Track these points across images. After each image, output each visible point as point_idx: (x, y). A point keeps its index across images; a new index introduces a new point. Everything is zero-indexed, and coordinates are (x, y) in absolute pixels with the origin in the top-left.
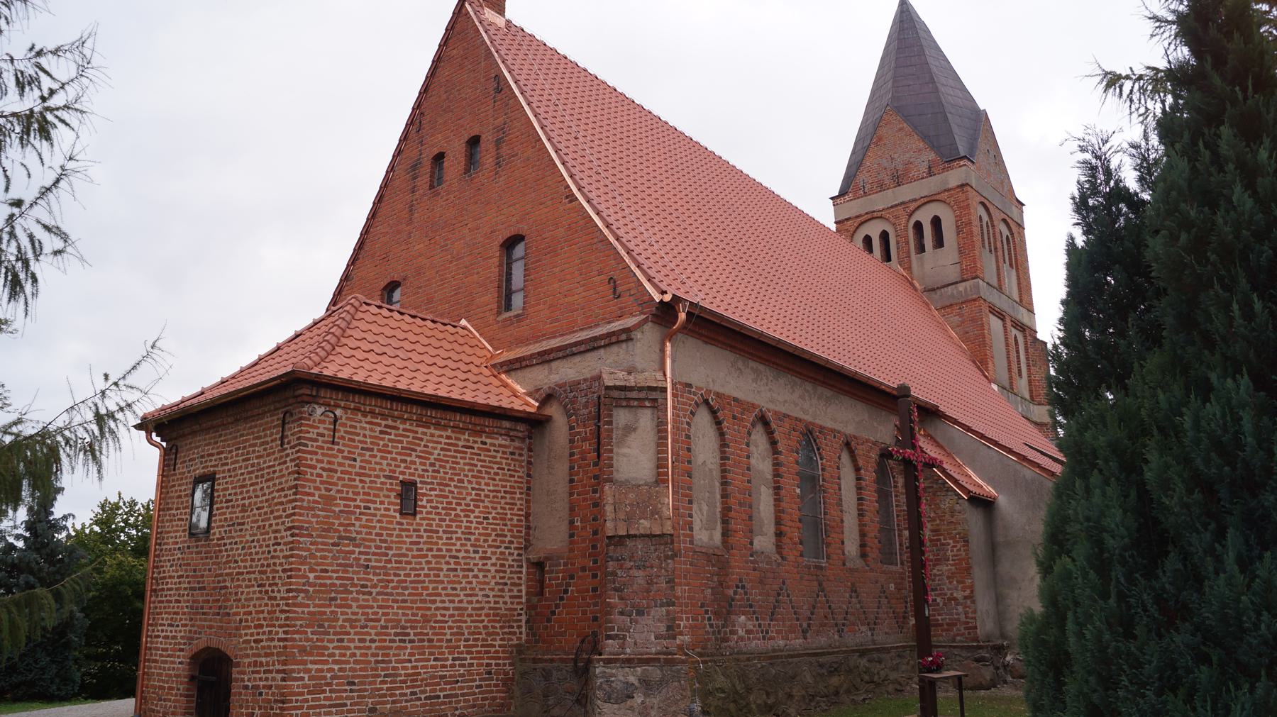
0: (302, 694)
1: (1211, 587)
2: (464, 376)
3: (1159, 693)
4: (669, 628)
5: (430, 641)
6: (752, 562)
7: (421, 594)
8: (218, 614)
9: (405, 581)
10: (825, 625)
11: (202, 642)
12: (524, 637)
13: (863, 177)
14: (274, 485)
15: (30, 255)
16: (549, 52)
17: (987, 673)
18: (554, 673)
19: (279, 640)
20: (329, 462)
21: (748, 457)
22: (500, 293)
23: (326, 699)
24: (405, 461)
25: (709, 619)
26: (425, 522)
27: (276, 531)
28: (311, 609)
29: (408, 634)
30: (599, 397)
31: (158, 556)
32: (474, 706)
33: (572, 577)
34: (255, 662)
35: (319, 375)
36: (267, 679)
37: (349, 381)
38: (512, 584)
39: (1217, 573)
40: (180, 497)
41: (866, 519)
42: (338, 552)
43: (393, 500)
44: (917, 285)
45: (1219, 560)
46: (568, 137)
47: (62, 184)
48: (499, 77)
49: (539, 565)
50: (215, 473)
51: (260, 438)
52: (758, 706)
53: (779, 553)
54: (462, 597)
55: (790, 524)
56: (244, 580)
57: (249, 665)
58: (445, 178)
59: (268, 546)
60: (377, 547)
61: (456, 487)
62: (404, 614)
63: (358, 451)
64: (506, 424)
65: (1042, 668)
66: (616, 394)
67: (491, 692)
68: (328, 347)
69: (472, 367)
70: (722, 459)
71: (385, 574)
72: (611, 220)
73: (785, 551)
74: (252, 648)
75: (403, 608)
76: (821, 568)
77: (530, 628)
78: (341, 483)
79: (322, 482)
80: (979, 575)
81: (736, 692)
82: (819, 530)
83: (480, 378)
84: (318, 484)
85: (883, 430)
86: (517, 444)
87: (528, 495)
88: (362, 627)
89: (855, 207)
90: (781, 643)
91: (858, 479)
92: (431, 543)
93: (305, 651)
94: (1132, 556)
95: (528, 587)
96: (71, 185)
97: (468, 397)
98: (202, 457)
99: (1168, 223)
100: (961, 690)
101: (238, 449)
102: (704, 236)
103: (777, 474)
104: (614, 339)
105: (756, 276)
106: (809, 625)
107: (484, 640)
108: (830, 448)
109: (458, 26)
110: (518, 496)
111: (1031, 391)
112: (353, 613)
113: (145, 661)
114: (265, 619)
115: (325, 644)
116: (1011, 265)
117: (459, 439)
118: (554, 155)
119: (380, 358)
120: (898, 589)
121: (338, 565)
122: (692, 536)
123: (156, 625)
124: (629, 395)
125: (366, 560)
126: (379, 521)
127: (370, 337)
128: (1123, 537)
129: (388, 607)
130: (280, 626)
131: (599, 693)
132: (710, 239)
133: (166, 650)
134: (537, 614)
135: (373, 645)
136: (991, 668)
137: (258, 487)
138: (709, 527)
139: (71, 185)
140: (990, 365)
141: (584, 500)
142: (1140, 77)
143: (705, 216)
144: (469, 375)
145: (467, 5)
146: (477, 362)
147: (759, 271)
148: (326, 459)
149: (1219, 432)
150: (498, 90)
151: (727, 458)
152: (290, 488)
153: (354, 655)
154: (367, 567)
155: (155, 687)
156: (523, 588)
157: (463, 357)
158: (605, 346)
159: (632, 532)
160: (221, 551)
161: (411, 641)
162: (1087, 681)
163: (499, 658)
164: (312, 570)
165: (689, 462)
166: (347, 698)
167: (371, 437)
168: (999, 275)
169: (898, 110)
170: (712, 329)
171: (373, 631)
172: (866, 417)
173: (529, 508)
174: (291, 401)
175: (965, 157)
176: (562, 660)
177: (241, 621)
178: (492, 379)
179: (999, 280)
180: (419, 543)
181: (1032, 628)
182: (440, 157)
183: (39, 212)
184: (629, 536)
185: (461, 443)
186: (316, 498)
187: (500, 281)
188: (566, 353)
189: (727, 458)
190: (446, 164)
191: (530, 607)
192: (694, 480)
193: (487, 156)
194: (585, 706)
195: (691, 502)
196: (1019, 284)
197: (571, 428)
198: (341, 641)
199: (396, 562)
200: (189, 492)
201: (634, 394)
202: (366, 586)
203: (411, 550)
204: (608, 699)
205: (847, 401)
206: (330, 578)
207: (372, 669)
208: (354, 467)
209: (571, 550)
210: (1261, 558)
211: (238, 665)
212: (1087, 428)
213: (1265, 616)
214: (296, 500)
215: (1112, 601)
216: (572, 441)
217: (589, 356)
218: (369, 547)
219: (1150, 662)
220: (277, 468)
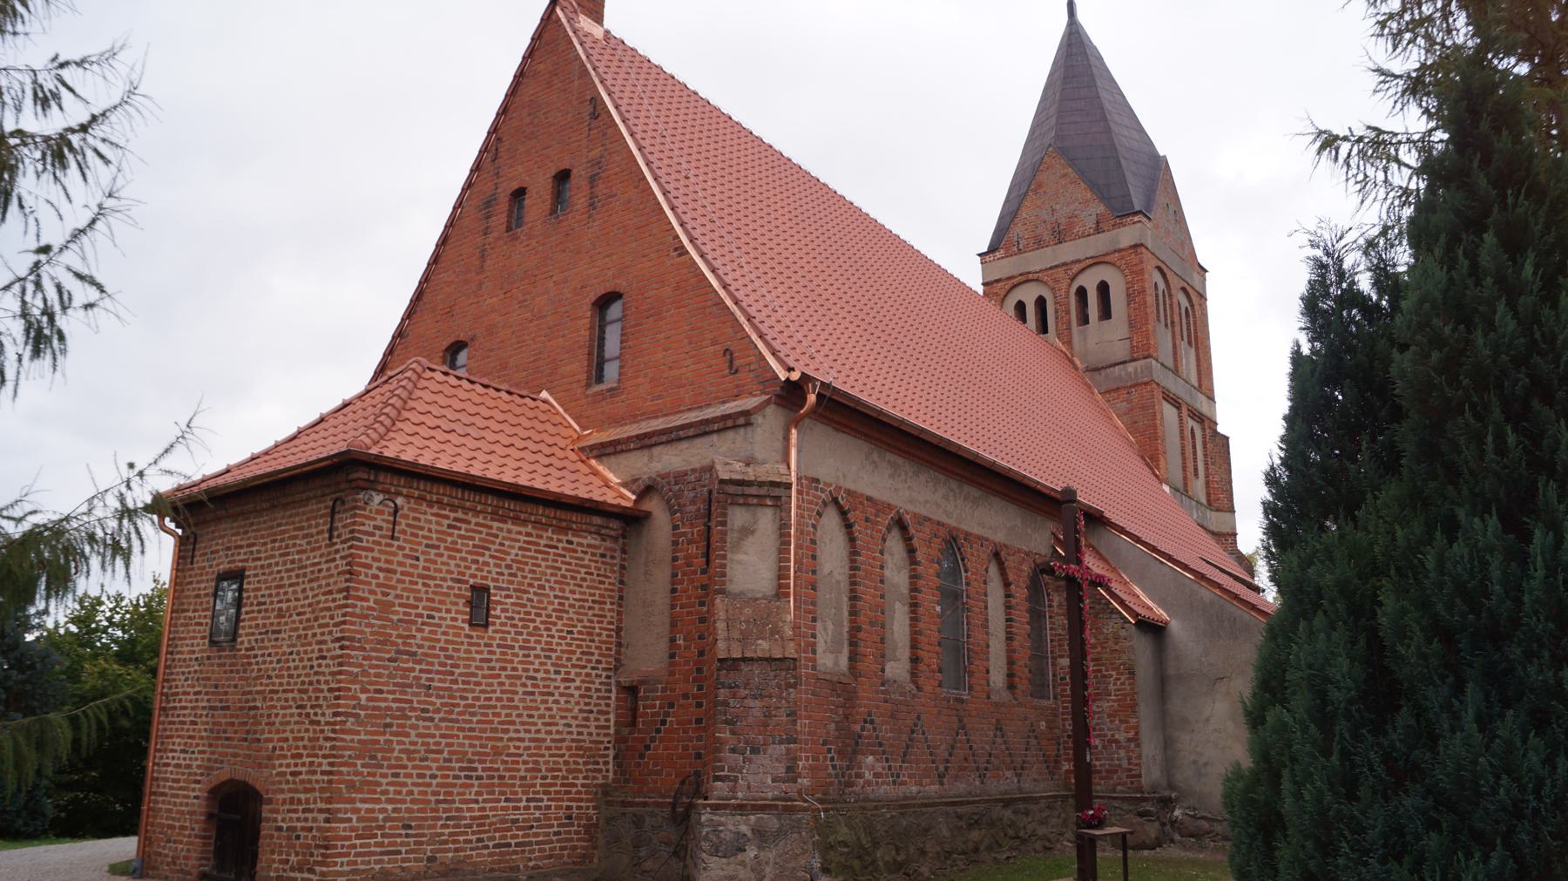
0: (349, 838)
1: (1446, 747)
2: (547, 461)
3: (1383, 861)
4: (789, 769)
5: (501, 777)
6: (883, 692)
7: (491, 722)
8: (245, 740)
9: (473, 706)
10: (965, 769)
11: (224, 773)
12: (611, 775)
13: (1017, 230)
14: (320, 586)
15: (57, 308)
16: (670, 81)
17: (1152, 830)
18: (648, 820)
19: (323, 773)
20: (387, 561)
21: (882, 567)
22: (590, 360)
23: (377, 845)
24: (477, 562)
25: (832, 759)
26: (498, 636)
27: (321, 642)
28: (363, 737)
29: (475, 769)
30: (710, 492)
31: (169, 667)
32: (551, 857)
33: (671, 706)
34: (292, 799)
35: (379, 457)
36: (306, 820)
37: (414, 464)
38: (599, 712)
39: (1453, 731)
40: (198, 596)
41: (1016, 643)
42: (396, 669)
43: (461, 608)
44: (1078, 362)
45: (1456, 716)
46: (678, 176)
47: (99, 225)
48: (596, 101)
49: (631, 691)
50: (243, 569)
51: (302, 528)
52: (886, 863)
53: (915, 682)
54: (540, 726)
55: (927, 647)
56: (279, 699)
57: (284, 802)
58: (526, 219)
59: (310, 660)
60: (441, 664)
61: (535, 594)
62: (471, 746)
63: (421, 548)
64: (597, 520)
65: (1251, 830)
66: (731, 489)
67: (572, 840)
68: (388, 422)
69: (555, 450)
70: (852, 569)
71: (451, 697)
72: (728, 279)
73: (921, 681)
74: (288, 782)
75: (470, 738)
76: (962, 701)
77: (619, 765)
78: (400, 586)
79: (378, 585)
80: (1146, 714)
81: (861, 846)
82: (961, 656)
83: (565, 463)
84: (373, 587)
85: (1037, 539)
86: (609, 544)
87: (620, 605)
88: (422, 760)
89: (1007, 267)
90: (914, 789)
91: (1008, 596)
92: (506, 661)
93: (353, 786)
94: (1358, 710)
95: (617, 716)
96: (109, 228)
97: (553, 487)
98: (228, 549)
99: (1418, 337)
100: (1125, 849)
101: (274, 541)
102: (833, 299)
103: (914, 589)
104: (730, 423)
105: (894, 350)
106: (946, 769)
107: (564, 778)
108: (976, 558)
109: (546, 36)
110: (608, 606)
111: (1208, 495)
112: (412, 743)
113: (152, 793)
114: (305, 747)
115: (378, 778)
116: (1190, 343)
117: (540, 537)
118: (661, 198)
119: (448, 437)
120: (1050, 728)
121: (395, 685)
122: (815, 660)
123: (165, 751)
124: (748, 491)
125: (429, 679)
126: (445, 633)
127: (436, 411)
128: (1349, 690)
129: (452, 736)
130: (324, 757)
131: (705, 845)
132: (841, 303)
133: (178, 781)
134: (628, 749)
135: (434, 782)
136: (1157, 824)
137: (299, 589)
138: (836, 652)
139: (109, 228)
140: (1162, 463)
141: (689, 613)
142: (1360, 139)
143: (836, 275)
144: (552, 460)
145: (558, 10)
146: (562, 443)
147: (897, 343)
148: (383, 557)
149: (1465, 577)
150: (595, 116)
151: (857, 569)
152: (340, 591)
153: (411, 793)
154: (429, 687)
155: (162, 826)
156: (612, 717)
157: (545, 436)
158: (719, 431)
159: (748, 655)
160: (250, 664)
161: (478, 778)
162: (1303, 847)
163: (581, 800)
164: (364, 691)
165: (814, 572)
166: (402, 844)
167: (437, 532)
168: (1175, 353)
169: (1063, 152)
170: (844, 414)
171: (434, 765)
172: (1019, 522)
173: (620, 621)
174: (343, 486)
175: (1140, 212)
176: (657, 804)
177: (274, 748)
178: (580, 465)
179: (1175, 360)
180: (490, 660)
181: (1240, 785)
182: (520, 194)
183: (71, 258)
184: (744, 659)
185: (543, 542)
186: (371, 604)
187: (591, 346)
188: (672, 437)
189: (857, 569)
190: (527, 202)
191: (620, 739)
192: (819, 594)
193: (578, 193)
194: (684, 859)
195: (814, 620)
196: (1198, 366)
197: (675, 527)
198: (396, 775)
199: (464, 682)
200: (211, 591)
201: (753, 490)
202: (427, 711)
203: (481, 668)
204: (715, 852)
205: (997, 503)
206: (385, 700)
207: (433, 810)
208: (416, 567)
209: (672, 673)
210: (1502, 716)
211: (270, 801)
212: (1311, 563)
213: (1505, 780)
214: (346, 606)
215: (1335, 759)
216: (675, 543)
217: (698, 442)
218: (432, 664)
219: (1374, 827)
220: (324, 566)
